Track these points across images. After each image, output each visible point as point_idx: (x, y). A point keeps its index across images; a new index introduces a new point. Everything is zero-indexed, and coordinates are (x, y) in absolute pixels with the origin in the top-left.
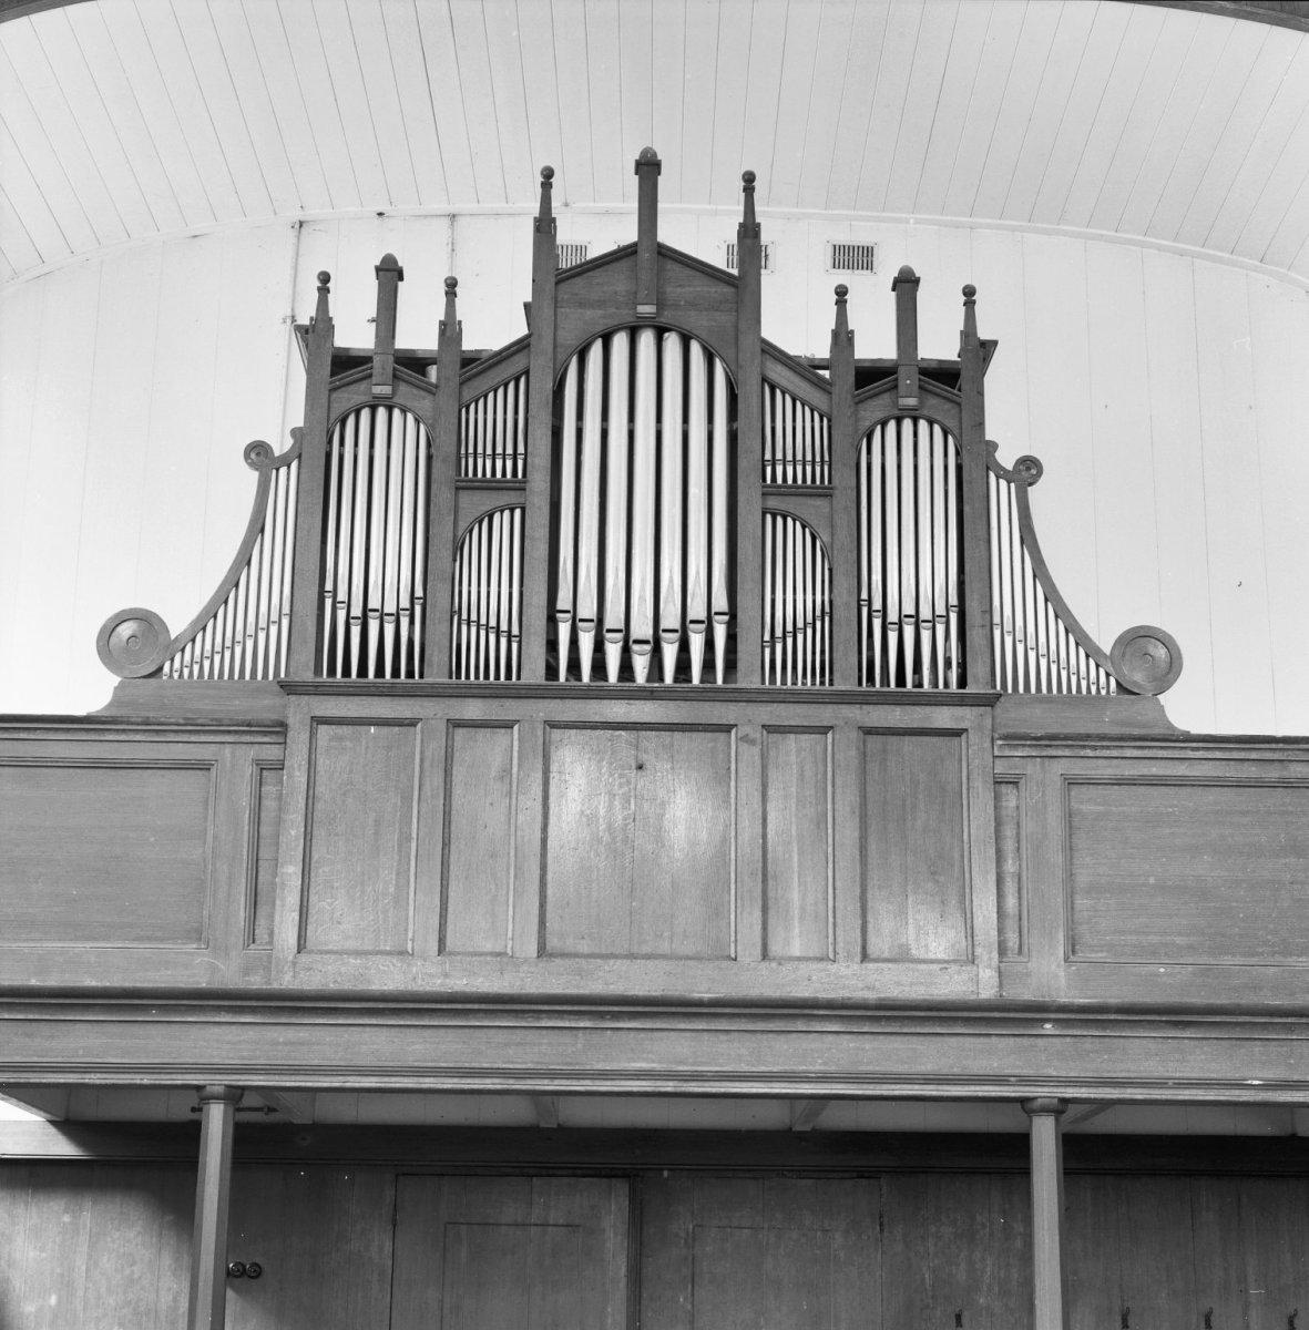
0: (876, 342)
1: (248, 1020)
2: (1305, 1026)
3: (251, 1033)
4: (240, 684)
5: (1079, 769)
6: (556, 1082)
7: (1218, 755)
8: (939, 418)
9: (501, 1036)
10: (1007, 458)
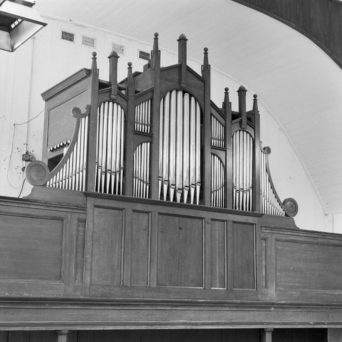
0: (235, 108)
1: (76, 308)
3: (76, 312)
4: (69, 191)
5: (279, 237)
6: (161, 326)
7: (306, 235)
8: (120, 103)
9: (146, 313)
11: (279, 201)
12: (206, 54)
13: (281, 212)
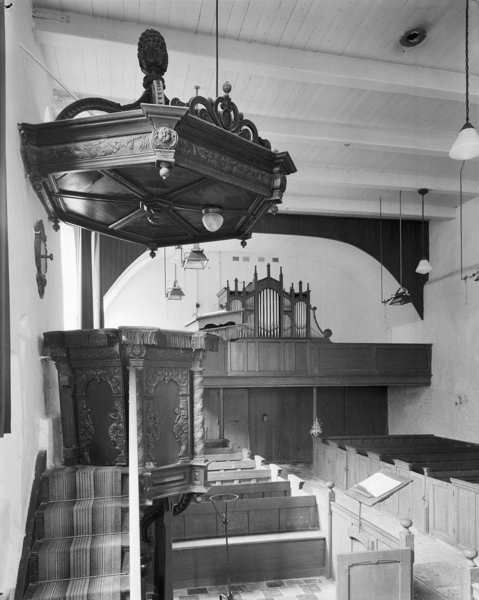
0: (297, 291)
2: (109, 223)
10: (312, 307)
11: (322, 332)
12: (281, 269)
13: (323, 336)
